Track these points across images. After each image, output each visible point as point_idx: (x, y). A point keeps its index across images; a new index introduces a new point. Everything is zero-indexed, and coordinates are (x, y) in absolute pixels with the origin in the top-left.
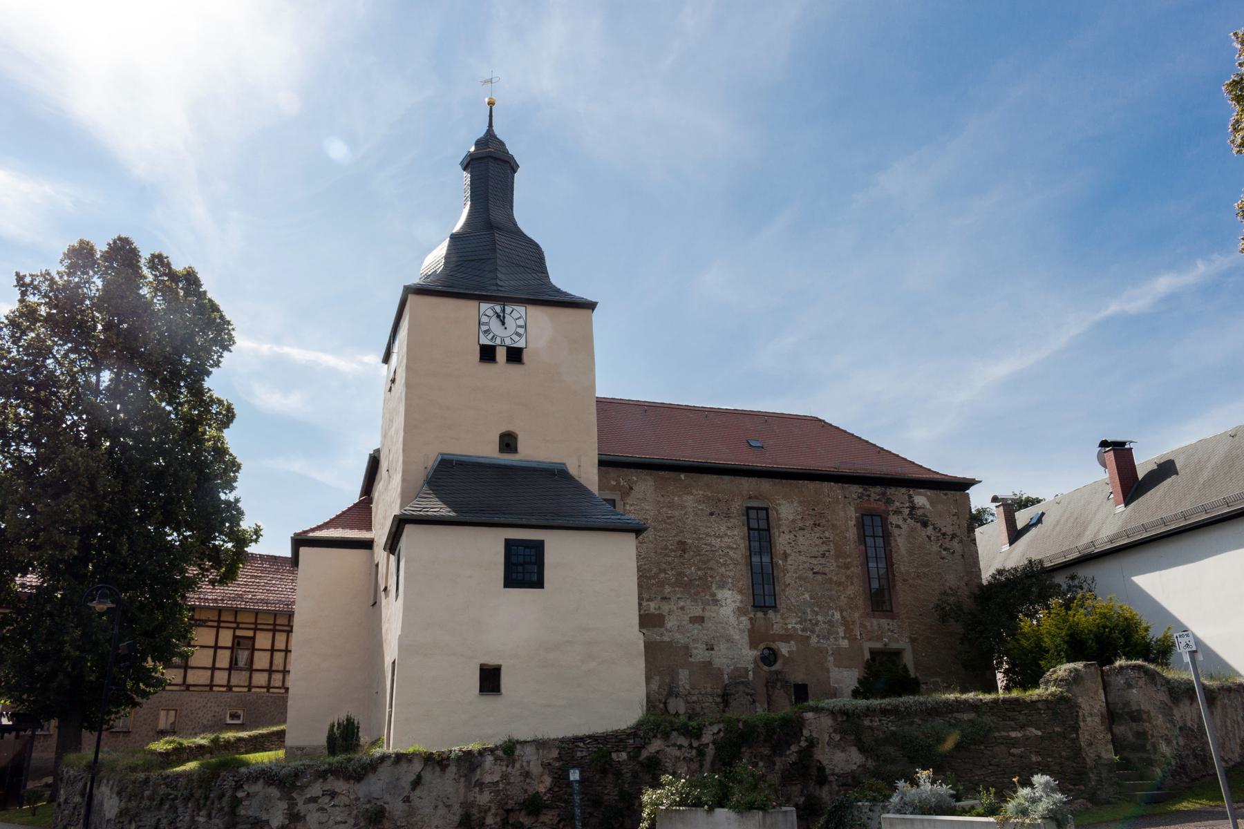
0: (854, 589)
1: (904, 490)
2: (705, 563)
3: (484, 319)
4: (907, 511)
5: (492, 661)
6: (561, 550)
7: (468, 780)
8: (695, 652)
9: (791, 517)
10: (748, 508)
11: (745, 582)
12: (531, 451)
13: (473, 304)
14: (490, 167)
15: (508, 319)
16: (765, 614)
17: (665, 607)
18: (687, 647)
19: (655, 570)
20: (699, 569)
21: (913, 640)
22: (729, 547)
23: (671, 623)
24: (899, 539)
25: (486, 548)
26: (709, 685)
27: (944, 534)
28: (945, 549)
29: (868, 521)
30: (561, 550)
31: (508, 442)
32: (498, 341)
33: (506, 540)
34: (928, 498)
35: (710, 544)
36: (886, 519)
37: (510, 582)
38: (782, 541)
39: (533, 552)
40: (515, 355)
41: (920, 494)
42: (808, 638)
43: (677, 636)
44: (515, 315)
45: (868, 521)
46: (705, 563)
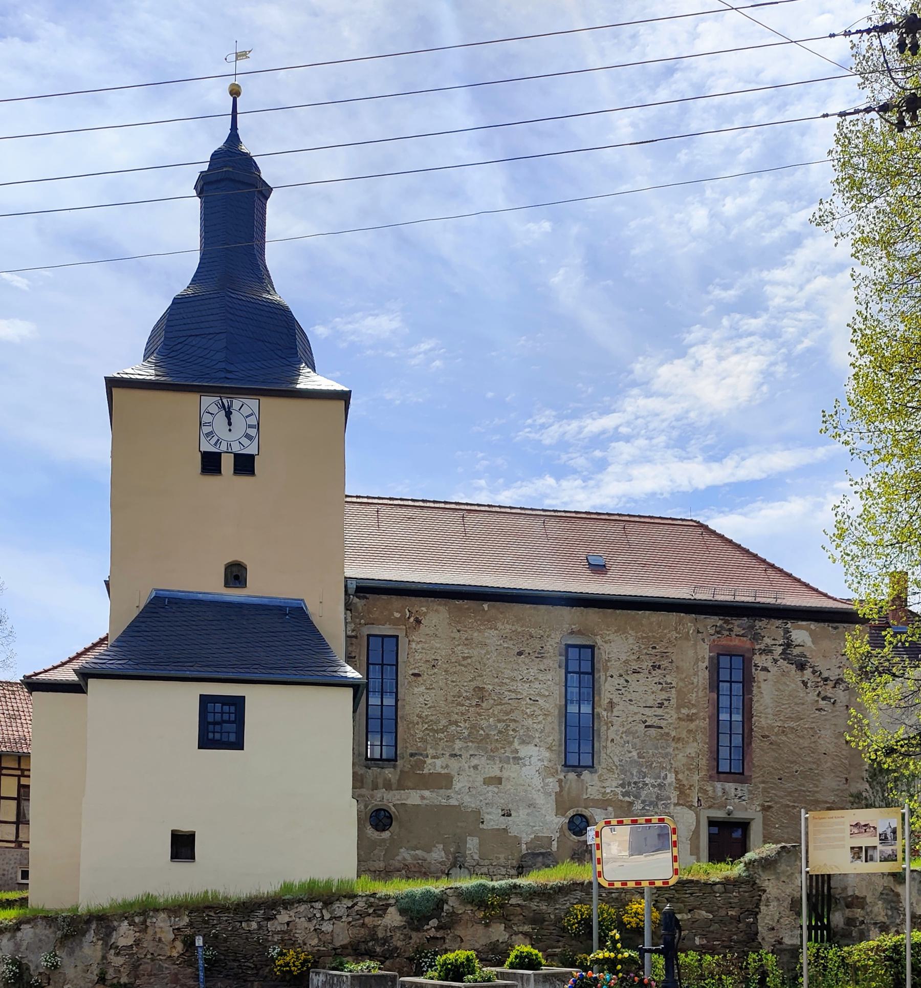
0: (696, 748)
1: (778, 622)
2: (507, 714)
3: (207, 418)
4: (780, 650)
5: (185, 828)
6: (264, 705)
7: (105, 943)
8: (487, 817)
9: (624, 657)
10: (568, 646)
11: (555, 736)
12: (261, 586)
13: (193, 398)
14: (233, 190)
15: (235, 416)
16: (579, 775)
17: (454, 764)
18: (478, 812)
19: (444, 722)
20: (499, 721)
21: (765, 809)
22: (539, 694)
23: (459, 784)
24: (763, 685)
25: (177, 705)
26: (502, 856)
27: (826, 679)
28: (824, 699)
29: (725, 661)
30: (264, 705)
31: (236, 574)
32: (223, 447)
33: (202, 697)
34: (812, 634)
35: (514, 691)
36: (751, 659)
37: (205, 743)
38: (608, 688)
39: (233, 709)
40: (245, 465)
41: (800, 628)
42: (631, 804)
43: (467, 799)
44: (246, 411)
45: (725, 661)
46: (507, 714)
